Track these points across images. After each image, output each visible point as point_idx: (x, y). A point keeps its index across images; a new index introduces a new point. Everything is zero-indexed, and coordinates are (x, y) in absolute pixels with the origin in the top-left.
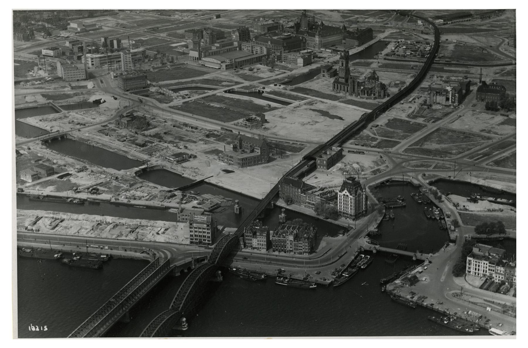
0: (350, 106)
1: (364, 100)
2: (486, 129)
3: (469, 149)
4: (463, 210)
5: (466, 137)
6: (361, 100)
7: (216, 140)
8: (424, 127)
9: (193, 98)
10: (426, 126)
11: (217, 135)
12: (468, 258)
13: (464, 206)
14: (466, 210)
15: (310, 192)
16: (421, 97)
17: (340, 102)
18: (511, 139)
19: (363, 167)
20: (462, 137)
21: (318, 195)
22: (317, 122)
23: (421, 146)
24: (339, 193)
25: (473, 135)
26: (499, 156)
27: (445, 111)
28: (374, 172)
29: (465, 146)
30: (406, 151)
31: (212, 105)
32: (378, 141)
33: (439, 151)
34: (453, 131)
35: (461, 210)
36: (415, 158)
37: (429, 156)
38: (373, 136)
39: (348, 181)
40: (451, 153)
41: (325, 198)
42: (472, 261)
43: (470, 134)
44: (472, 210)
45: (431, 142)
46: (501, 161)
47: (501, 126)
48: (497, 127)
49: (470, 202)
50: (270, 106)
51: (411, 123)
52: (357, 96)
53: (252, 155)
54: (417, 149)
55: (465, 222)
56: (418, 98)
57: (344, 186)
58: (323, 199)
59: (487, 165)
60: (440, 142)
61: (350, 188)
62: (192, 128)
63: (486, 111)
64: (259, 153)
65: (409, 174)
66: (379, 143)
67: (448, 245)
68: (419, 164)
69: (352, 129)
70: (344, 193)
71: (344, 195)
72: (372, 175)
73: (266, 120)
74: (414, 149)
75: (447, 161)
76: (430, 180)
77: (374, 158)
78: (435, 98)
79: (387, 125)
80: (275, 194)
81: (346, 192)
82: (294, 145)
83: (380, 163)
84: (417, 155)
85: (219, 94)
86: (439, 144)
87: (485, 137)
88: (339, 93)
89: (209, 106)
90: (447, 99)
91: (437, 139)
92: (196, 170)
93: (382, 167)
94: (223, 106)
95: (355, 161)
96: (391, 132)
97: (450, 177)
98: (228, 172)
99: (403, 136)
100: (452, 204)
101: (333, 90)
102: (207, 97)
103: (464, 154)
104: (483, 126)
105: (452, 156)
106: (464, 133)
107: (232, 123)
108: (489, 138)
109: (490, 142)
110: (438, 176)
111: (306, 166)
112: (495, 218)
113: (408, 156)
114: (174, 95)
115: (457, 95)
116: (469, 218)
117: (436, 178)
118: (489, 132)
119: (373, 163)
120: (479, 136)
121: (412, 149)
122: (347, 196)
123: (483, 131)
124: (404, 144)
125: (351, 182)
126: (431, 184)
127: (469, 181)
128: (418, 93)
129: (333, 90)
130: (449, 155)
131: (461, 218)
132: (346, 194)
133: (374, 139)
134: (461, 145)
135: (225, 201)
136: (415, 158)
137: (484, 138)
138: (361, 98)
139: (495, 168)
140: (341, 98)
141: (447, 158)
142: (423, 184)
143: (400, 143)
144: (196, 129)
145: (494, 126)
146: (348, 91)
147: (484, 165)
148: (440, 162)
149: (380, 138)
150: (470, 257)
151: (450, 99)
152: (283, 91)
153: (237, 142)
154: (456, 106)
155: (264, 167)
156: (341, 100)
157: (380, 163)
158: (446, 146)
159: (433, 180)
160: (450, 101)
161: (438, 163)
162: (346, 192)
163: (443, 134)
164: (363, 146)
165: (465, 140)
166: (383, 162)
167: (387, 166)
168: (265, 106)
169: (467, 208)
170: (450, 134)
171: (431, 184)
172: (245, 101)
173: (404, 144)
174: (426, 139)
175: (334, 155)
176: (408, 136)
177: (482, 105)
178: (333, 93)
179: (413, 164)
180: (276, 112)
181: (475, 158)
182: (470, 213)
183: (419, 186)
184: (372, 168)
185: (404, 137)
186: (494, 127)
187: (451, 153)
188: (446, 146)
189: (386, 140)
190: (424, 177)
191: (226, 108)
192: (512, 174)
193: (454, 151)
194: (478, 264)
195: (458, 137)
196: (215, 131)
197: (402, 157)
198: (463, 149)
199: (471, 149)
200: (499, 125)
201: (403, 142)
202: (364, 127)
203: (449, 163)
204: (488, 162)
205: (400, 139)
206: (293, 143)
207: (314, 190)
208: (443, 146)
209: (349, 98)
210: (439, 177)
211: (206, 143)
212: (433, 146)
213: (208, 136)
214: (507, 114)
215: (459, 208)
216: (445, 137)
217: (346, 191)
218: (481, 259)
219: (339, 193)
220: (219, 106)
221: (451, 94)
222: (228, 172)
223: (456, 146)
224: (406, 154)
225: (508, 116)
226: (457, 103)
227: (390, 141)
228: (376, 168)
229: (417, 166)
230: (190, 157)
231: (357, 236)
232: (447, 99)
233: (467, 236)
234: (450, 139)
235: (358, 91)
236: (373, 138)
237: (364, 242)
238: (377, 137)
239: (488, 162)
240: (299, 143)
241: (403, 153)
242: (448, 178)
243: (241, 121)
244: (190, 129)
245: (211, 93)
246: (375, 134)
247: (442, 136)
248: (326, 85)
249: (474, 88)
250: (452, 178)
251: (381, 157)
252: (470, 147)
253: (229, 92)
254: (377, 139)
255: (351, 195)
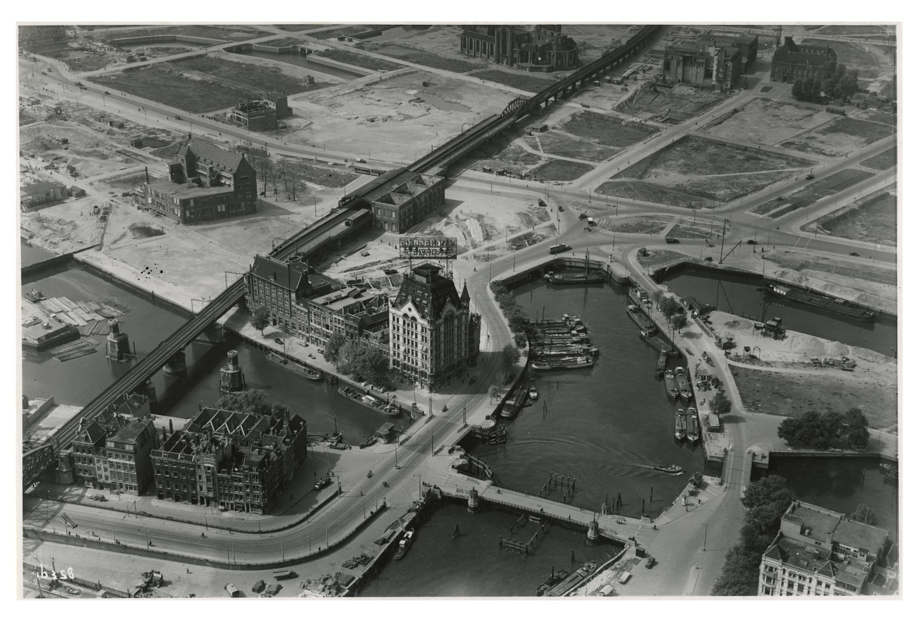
0: (491, 84)
1: (527, 73)
2: (796, 140)
3: (758, 188)
4: (745, 361)
5: (748, 159)
6: (519, 72)
7: (154, 153)
8: (652, 132)
9: (151, 61)
10: (657, 130)
11: (163, 141)
12: (767, 561)
13: (747, 349)
14: (753, 359)
15: (320, 300)
16: (651, 68)
17: (472, 75)
18: (35, 287)
19: (492, 227)
20: (741, 157)
21: (339, 312)
22: (410, 117)
23: (641, 177)
24: (392, 310)
25: (765, 153)
26: (833, 208)
27: (700, 100)
28: (517, 243)
29: (746, 180)
30: (603, 188)
31: (186, 75)
32: (541, 163)
33: (685, 191)
34: (721, 145)
35: (738, 358)
36: (624, 207)
37: (661, 201)
38: (530, 150)
39: (418, 278)
40: (713, 197)
41: (354, 320)
42: (780, 572)
43: (758, 151)
44: (771, 359)
45: (667, 168)
46: (838, 218)
47: (830, 135)
48: (821, 137)
49: (765, 335)
50: (311, 80)
51: (623, 124)
52: (512, 65)
53: (215, 191)
54: (635, 183)
55: (751, 404)
56: (644, 71)
57: (408, 286)
58: (351, 323)
59: (803, 228)
60: (687, 169)
61: (422, 298)
62: (111, 124)
63: (795, 102)
64: (232, 189)
65: (604, 248)
66: (544, 167)
67: (701, 485)
68: (632, 222)
69: (483, 133)
70: (405, 309)
71: (405, 315)
72: (510, 249)
73: (290, 109)
74: (623, 184)
75: (703, 216)
76: (658, 267)
77: (523, 207)
78: (680, 71)
79: (568, 127)
80: (237, 297)
81: (409, 308)
82: (336, 169)
83: (536, 219)
84: (631, 200)
85: (212, 55)
86: (685, 173)
87: (794, 159)
88: (475, 57)
89: (180, 79)
90: (708, 75)
91: (682, 161)
92: (68, 229)
93: (540, 229)
94: (209, 78)
95: (475, 212)
96: (574, 142)
97: (710, 259)
98: (147, 232)
99: (601, 153)
100: (714, 340)
101: (462, 52)
102: (189, 58)
103: (745, 199)
104: (788, 134)
105: (717, 203)
106: (746, 149)
107: (211, 114)
108: (804, 163)
109: (807, 171)
110: (680, 256)
111: (343, 224)
112: (836, 390)
113: (606, 200)
114: (113, 53)
115: (730, 64)
116: (763, 389)
117: (674, 263)
118: (803, 148)
119: (518, 217)
120: (780, 156)
121: (618, 184)
122: (414, 319)
123: (788, 144)
124: (602, 171)
125: (424, 280)
126: (659, 277)
127: (758, 271)
128: (645, 62)
129: (462, 52)
130: (709, 202)
131: (738, 385)
132: (410, 314)
133: (530, 158)
134: (737, 177)
135: (99, 318)
136: (624, 207)
137: (791, 161)
138: (519, 67)
139: (824, 237)
140: (476, 67)
141: (704, 209)
142: (637, 276)
143: (593, 168)
144: (121, 126)
145: (813, 134)
146: (492, 54)
147: (795, 228)
148: (686, 218)
149: (545, 156)
150: (772, 555)
151: (714, 73)
152: (355, 50)
153: (180, 159)
154: (727, 90)
155: (239, 224)
156: (474, 71)
157: (536, 219)
158: (703, 178)
159: (666, 266)
160: (714, 78)
161: (682, 222)
162: (409, 308)
163: (696, 150)
164: (501, 173)
165: (747, 165)
166: (544, 217)
167: (557, 227)
168: (301, 81)
169: (756, 354)
170: (712, 150)
171: (659, 277)
172: (265, 69)
173: (602, 171)
174: (655, 160)
175: (419, 197)
176: (613, 153)
177: (783, 91)
178: (461, 58)
179: (618, 224)
180: (324, 93)
181: (771, 212)
182: (764, 368)
183: (627, 284)
184: (512, 231)
185: (602, 156)
186: (813, 138)
187: (713, 197)
188: (703, 178)
189: (559, 162)
190: (644, 259)
191: (213, 83)
192: (888, 260)
193: (722, 192)
194: (796, 581)
195: (732, 157)
196: (164, 131)
197: (594, 203)
198: (743, 186)
199: (763, 187)
200: (824, 132)
201: (600, 166)
202: (515, 130)
203: (708, 222)
204: (803, 222)
205: (592, 159)
206: (335, 164)
207: (332, 296)
208: (695, 178)
209: (494, 67)
210: (681, 260)
211: (129, 158)
212: (668, 177)
213: (139, 144)
214: (842, 109)
215: (733, 352)
216: (701, 158)
217: (410, 305)
218: (809, 568)
219: (392, 310)
220: (198, 78)
221: (716, 62)
222: (147, 232)
223: (727, 179)
224: (604, 197)
225: (843, 113)
226: (729, 84)
227: (570, 163)
228: (525, 231)
229: (626, 228)
230: (70, 194)
231: (427, 445)
232: (708, 75)
233: (756, 449)
234: (711, 161)
235: (513, 52)
236: (529, 155)
237: (443, 472)
238: (541, 153)
239: (803, 222)
240: (348, 164)
241: (596, 195)
242: (705, 264)
243: (229, 112)
244: (108, 127)
245: (197, 51)
246: (535, 147)
247: (694, 154)
248: (450, 41)
249: (766, 56)
250: (715, 262)
251: (542, 204)
252: (758, 183)
253: (239, 50)
254: (539, 158)
255: (423, 317)
